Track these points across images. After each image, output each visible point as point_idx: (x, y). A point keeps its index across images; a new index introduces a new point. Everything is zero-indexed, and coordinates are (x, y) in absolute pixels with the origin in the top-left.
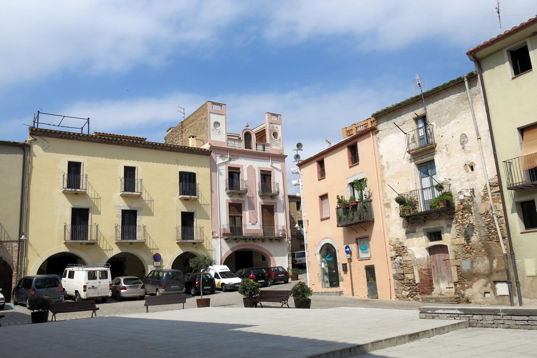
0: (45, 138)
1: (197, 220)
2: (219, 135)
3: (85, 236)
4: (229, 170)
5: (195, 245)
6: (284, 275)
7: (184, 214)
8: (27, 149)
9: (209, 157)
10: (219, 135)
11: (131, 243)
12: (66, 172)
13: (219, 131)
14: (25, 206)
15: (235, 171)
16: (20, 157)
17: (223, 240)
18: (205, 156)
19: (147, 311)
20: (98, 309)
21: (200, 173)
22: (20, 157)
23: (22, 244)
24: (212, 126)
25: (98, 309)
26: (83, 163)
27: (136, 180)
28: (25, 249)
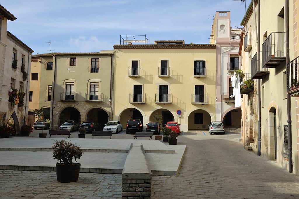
0: (121, 50)
1: (217, 87)
2: (224, 33)
3: (140, 100)
4: (231, 57)
5: (204, 106)
6: (151, 131)
7: (196, 87)
8: (113, 56)
9: (215, 49)
10: (224, 33)
11: (165, 104)
12: (131, 66)
13: (224, 31)
14: (112, 85)
15: (235, 56)
16: (110, 58)
17: (224, 103)
18: (212, 49)
19: (93, 138)
20: (71, 135)
21: (209, 61)
22: (110, 58)
23: (112, 105)
24: (219, 28)
25: (71, 135)
26: (139, 60)
27: (168, 68)
28: (257, 35)
